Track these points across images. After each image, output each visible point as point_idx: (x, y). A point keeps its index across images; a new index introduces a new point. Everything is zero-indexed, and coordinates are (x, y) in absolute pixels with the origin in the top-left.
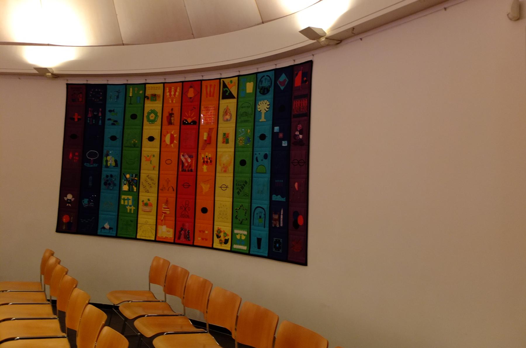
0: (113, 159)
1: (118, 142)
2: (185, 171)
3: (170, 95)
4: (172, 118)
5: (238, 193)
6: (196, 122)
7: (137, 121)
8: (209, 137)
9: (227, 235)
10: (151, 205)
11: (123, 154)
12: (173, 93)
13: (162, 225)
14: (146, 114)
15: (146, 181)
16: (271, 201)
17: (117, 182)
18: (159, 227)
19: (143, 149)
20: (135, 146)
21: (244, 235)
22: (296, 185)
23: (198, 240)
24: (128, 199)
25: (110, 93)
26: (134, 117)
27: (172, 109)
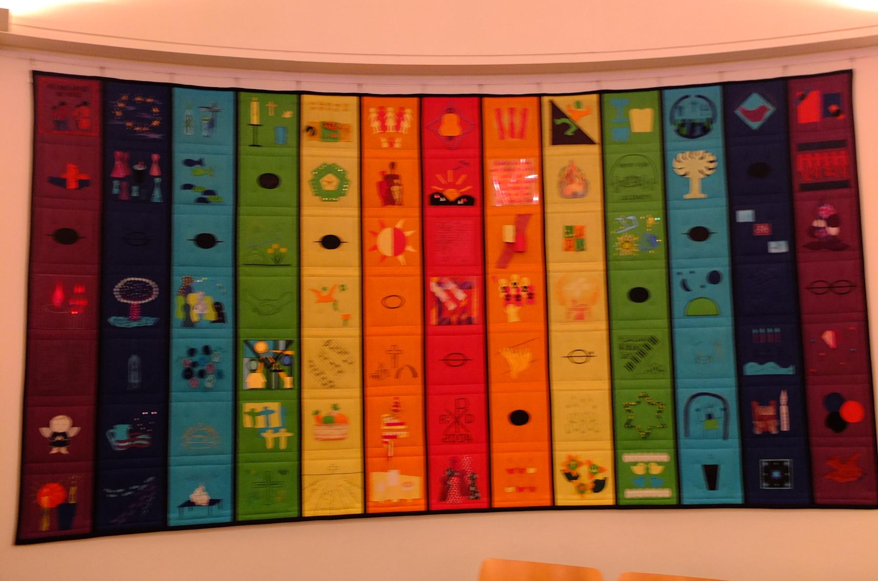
0: (209, 301)
1: (222, 253)
2: (450, 323)
3: (384, 127)
4: (395, 189)
5: (630, 367)
6: (475, 200)
7: (284, 192)
8: (520, 234)
9: (601, 470)
10: (343, 421)
11: (242, 287)
12: (391, 123)
13: (385, 469)
14: (307, 175)
15: (323, 357)
16: (743, 382)
17: (227, 368)
18: (375, 477)
19: (306, 271)
20: (278, 262)
21: (659, 463)
22: (828, 337)
23: (505, 492)
24: (267, 412)
25: (184, 110)
26: (269, 181)
27: (393, 165)
